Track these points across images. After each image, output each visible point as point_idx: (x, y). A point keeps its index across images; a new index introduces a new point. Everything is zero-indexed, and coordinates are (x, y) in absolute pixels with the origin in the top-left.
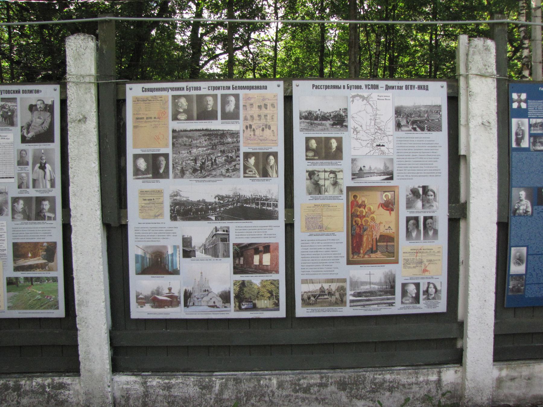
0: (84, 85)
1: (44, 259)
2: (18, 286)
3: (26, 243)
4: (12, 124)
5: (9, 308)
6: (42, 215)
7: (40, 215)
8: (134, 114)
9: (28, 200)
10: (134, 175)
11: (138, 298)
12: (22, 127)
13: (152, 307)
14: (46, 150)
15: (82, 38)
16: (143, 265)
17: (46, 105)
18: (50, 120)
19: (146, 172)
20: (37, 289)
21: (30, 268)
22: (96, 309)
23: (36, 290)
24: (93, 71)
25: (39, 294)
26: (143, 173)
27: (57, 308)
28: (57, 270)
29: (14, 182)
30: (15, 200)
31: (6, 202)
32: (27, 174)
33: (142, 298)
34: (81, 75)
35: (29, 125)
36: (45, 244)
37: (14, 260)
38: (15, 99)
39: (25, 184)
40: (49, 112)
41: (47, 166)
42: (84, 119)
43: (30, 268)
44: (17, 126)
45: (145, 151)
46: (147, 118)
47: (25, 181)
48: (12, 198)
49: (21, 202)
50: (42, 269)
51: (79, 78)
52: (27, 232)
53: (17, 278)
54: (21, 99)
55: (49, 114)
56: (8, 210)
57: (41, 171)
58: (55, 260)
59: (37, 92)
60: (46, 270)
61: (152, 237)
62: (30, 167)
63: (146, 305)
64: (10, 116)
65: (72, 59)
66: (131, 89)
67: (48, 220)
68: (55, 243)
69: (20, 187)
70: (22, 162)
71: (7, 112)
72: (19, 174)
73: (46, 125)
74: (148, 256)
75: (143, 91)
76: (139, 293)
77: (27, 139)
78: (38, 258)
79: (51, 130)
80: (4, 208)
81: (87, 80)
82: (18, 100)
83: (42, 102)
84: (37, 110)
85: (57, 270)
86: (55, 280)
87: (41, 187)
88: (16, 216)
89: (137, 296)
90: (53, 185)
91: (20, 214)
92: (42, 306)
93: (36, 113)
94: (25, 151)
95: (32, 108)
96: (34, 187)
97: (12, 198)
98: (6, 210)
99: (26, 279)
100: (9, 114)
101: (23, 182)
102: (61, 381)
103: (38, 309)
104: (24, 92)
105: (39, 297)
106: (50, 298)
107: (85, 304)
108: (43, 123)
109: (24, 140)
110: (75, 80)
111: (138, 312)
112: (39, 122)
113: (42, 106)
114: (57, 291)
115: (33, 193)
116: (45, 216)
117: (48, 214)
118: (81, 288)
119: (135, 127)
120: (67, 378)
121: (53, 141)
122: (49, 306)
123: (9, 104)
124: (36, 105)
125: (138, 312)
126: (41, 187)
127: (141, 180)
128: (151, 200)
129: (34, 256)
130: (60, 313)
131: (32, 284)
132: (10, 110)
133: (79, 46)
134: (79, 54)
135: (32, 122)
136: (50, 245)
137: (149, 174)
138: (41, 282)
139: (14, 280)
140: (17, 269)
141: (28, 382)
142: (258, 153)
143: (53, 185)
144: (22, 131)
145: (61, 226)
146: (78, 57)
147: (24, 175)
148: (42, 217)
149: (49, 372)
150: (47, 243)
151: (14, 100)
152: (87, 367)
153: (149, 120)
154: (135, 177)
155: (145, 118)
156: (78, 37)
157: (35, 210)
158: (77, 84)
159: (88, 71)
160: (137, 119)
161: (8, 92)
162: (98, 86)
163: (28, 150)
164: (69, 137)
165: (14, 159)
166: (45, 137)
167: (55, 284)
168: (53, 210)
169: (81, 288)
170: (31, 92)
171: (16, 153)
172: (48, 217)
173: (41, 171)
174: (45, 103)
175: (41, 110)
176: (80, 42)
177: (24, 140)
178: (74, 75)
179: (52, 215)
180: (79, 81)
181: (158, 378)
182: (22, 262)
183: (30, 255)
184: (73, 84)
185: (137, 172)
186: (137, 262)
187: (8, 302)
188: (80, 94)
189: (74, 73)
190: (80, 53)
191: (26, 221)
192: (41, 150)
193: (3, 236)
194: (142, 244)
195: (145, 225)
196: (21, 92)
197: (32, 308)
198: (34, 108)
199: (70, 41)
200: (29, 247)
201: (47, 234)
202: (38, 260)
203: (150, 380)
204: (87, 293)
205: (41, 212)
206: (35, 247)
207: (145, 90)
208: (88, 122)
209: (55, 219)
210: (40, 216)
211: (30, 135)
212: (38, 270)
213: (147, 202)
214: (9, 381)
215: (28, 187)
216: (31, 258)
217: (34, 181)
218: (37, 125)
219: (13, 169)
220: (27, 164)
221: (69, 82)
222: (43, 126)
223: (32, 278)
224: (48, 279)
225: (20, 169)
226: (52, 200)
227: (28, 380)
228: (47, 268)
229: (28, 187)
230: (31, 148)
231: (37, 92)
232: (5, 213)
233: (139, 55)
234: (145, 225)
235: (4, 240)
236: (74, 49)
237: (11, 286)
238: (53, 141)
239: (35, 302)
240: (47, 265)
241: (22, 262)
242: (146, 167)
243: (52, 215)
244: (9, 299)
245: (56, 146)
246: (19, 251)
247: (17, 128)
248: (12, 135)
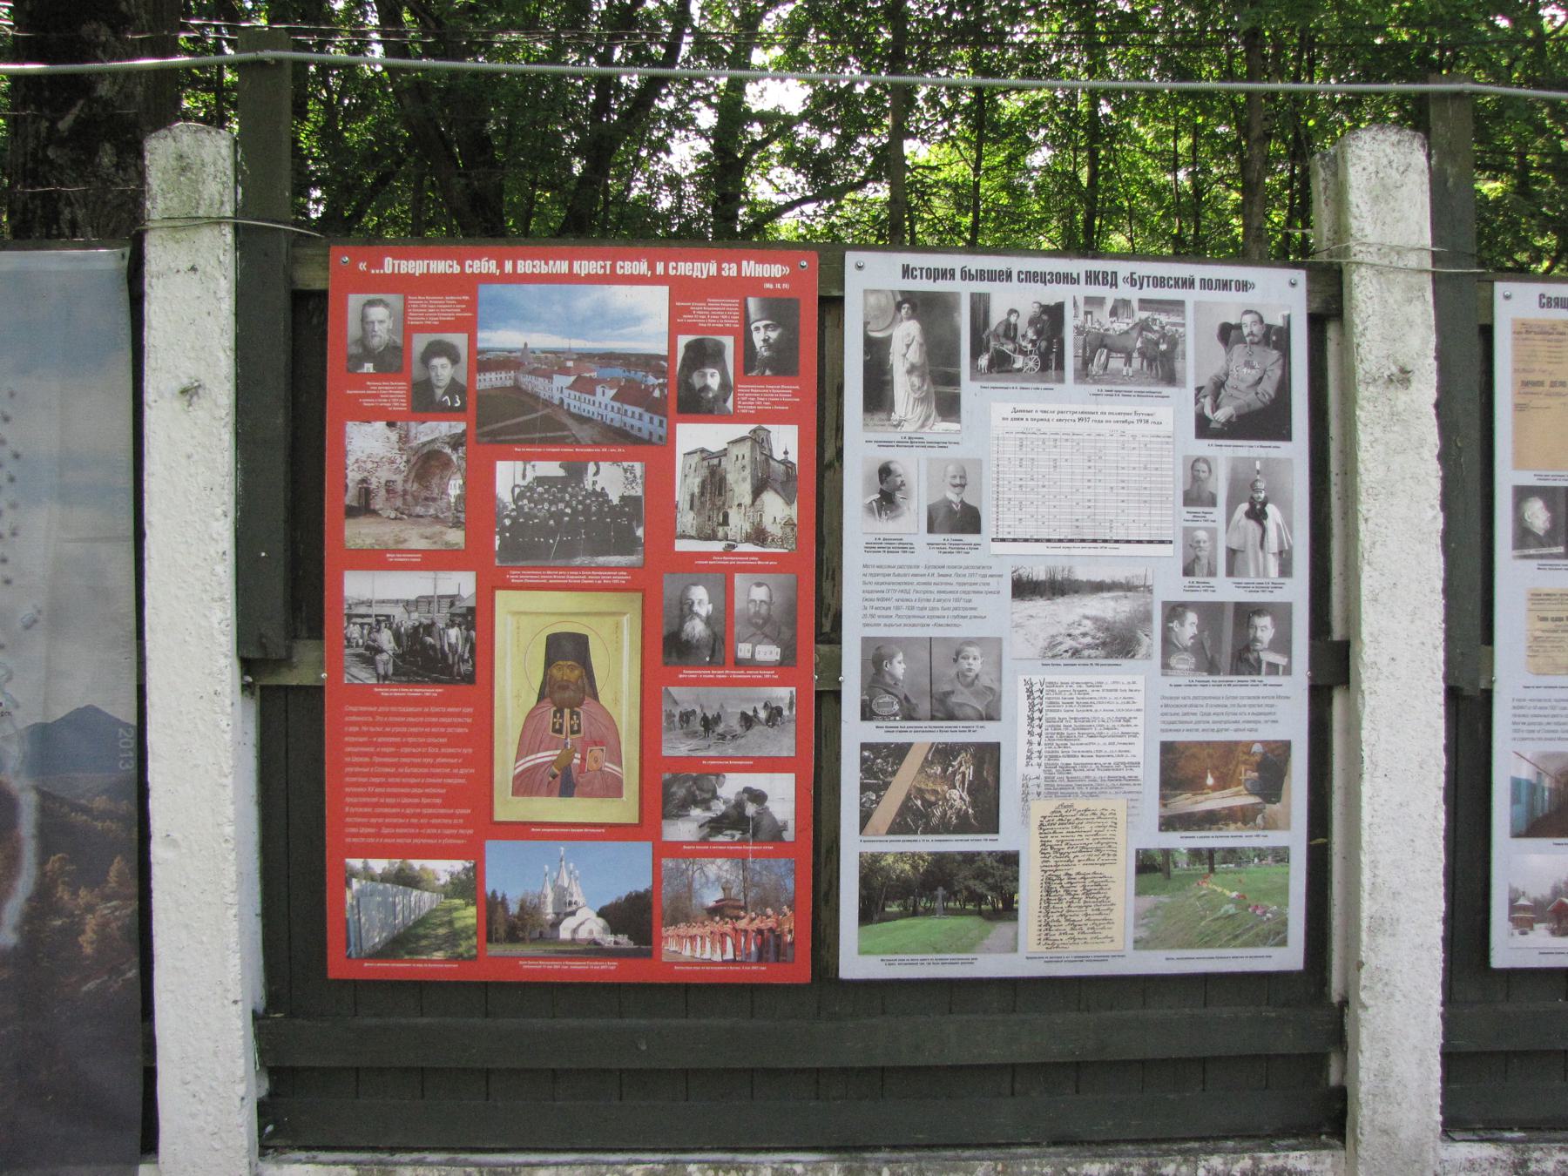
0: (1402, 275)
1: (1251, 793)
2: (1168, 875)
3: (1200, 744)
4: (1171, 378)
5: (1139, 943)
6: (1251, 657)
7: (1247, 660)
8: (1516, 371)
9: (1210, 612)
10: (1515, 547)
11: (1513, 907)
12: (1199, 390)
13: (1553, 933)
14: (1267, 462)
15: (1395, 138)
16: (1531, 807)
17: (1269, 327)
18: (1278, 372)
19: (1550, 538)
20: (1224, 886)
21: (1210, 820)
22: (1418, 941)
23: (1223, 888)
24: (1427, 240)
25: (1231, 901)
26: (1541, 542)
27: (1283, 943)
28: (1287, 827)
29: (1173, 555)
30: (1174, 611)
31: (1147, 618)
32: (1212, 533)
33: (1524, 908)
34: (1392, 248)
35: (1219, 385)
36: (1257, 748)
37: (1163, 797)
38: (1181, 303)
39: (1204, 561)
40: (1275, 348)
41: (1271, 509)
42: (1403, 377)
43: (1210, 820)
44: (1183, 384)
45: (1546, 478)
46: (1553, 384)
47: (1204, 555)
48: (1165, 604)
49: (1192, 617)
50: (1245, 823)
51: (1386, 255)
52: (1204, 710)
53: (1167, 853)
54: (1197, 304)
55: (1275, 354)
56: (1153, 641)
57: (1252, 524)
58: (1284, 798)
59: (1244, 286)
60: (1256, 827)
61: (1558, 728)
62: (1219, 512)
63: (1536, 926)
64: (1163, 354)
65: (1366, 198)
66: (1507, 297)
67: (1268, 674)
68: (1286, 746)
69: (1188, 571)
70: (1196, 496)
71: (1157, 344)
72: (1188, 532)
73: (1269, 388)
74: (1547, 783)
75: (1542, 306)
76: (1516, 891)
77: (1213, 425)
78: (1234, 789)
79: (1296, 405)
80: (1140, 634)
81: (1412, 261)
82: (1189, 308)
83: (1256, 317)
84: (1241, 340)
85: (1287, 827)
86: (1281, 855)
87: (1252, 574)
88: (1173, 661)
89: (1512, 901)
90: (1285, 570)
91: (1186, 656)
92: (1236, 937)
93: (1238, 349)
94: (1206, 461)
95: (1228, 333)
96: (1230, 572)
97: (1165, 604)
98: (1145, 641)
99: (1196, 854)
100: (1163, 347)
101: (1198, 557)
102: (1279, 1163)
103: (1226, 945)
104: (1207, 284)
105: (1230, 909)
106: (1264, 913)
107: (1387, 927)
108: (1261, 379)
109: (1204, 428)
110: (1375, 259)
111: (1512, 948)
112: (1249, 376)
113: (1256, 329)
114: (1284, 890)
115: (1226, 591)
116: (1259, 661)
117: (1268, 657)
118: (1379, 880)
119: (1519, 408)
120: (1297, 1153)
121: (1286, 435)
122: (1257, 935)
123: (1163, 318)
124: (1239, 327)
125: (1512, 948)
126: (1252, 574)
127: (1534, 563)
128: (1561, 619)
129: (1223, 783)
130: (1290, 957)
131: (1212, 870)
132: (1164, 336)
133: (1385, 161)
134: (1384, 186)
135: (1227, 375)
136: (1272, 751)
137: (1556, 545)
138: (1238, 865)
139: (1160, 859)
140: (1169, 823)
141: (1184, 1169)
142: (1554, 489)
143: (1285, 570)
144: (1197, 401)
145: (1306, 693)
146: (1383, 193)
147: (1202, 535)
148: (1251, 665)
149: (1227, 1138)
150: (1263, 743)
151: (1177, 306)
152: (1380, 1119)
153: (1559, 389)
154: (1517, 553)
155: (1547, 383)
156: (1380, 137)
157: (1230, 644)
158: (1379, 270)
159: (1415, 237)
160: (1526, 384)
161: (1160, 282)
162: (1437, 279)
163: (1215, 459)
164: (1360, 426)
165: (1175, 483)
166: (1266, 422)
167: (1279, 868)
168: (1282, 643)
169: (1379, 880)
170: (1225, 285)
171: (1180, 472)
172: (1269, 664)
173: (1252, 525)
174: (1267, 321)
175: (1252, 343)
176: (1389, 150)
177: (1204, 428)
178: (1370, 245)
179: (1280, 660)
180: (1386, 262)
181: (1561, 1149)
182: (1187, 803)
183: (1210, 781)
184: (1370, 272)
185: (1524, 536)
186: (1515, 800)
187: (1136, 926)
188: (1391, 301)
189: (1371, 239)
190: (1389, 182)
191: (1205, 677)
192: (1252, 460)
193: (1133, 722)
194: (1531, 749)
195: (1543, 694)
196: (1197, 284)
197: (1207, 944)
198: (1233, 333)
199: (1361, 144)
200: (1210, 756)
201: (1262, 718)
202: (1237, 794)
203: (1537, 1155)
204: (1395, 895)
205: (1248, 648)
206: (1225, 759)
207: (1547, 302)
208: (1414, 385)
209: (1288, 671)
210: (1244, 661)
211: (1222, 415)
212: (1232, 826)
213: (1549, 625)
214: (1129, 1165)
215: (1212, 573)
216: (1214, 789)
217: (1232, 553)
218: (1243, 386)
219: (1171, 517)
220: (1213, 502)
221: (1359, 264)
222: (1259, 389)
223: (1211, 852)
224: (1260, 853)
225: (1190, 517)
226: (1281, 614)
227: (1186, 1161)
228: (1259, 819)
229: (1212, 573)
230: (1225, 454)
231: (1244, 286)
232: (1142, 651)
233: (497, 163)
234: (1543, 694)
235: (1135, 735)
236: (1372, 169)
237: (1149, 878)
238: (1286, 435)
239: (1215, 926)
240: (1260, 811)
241: (1187, 803)
242: (1548, 525)
243: (1280, 660)
244: (1141, 917)
245: (1295, 452)
246: (1179, 767)
247: (1183, 390)
248: (1171, 412)
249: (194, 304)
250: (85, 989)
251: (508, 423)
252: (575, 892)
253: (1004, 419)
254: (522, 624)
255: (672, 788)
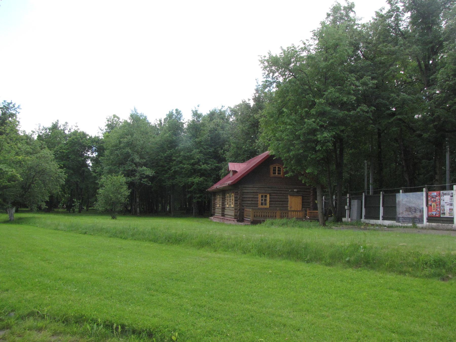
249: (424, 193)
250: (160, 205)
251: (381, 197)
252: (434, 213)
253: (445, 197)
254: (433, 204)
255: (437, 210)
